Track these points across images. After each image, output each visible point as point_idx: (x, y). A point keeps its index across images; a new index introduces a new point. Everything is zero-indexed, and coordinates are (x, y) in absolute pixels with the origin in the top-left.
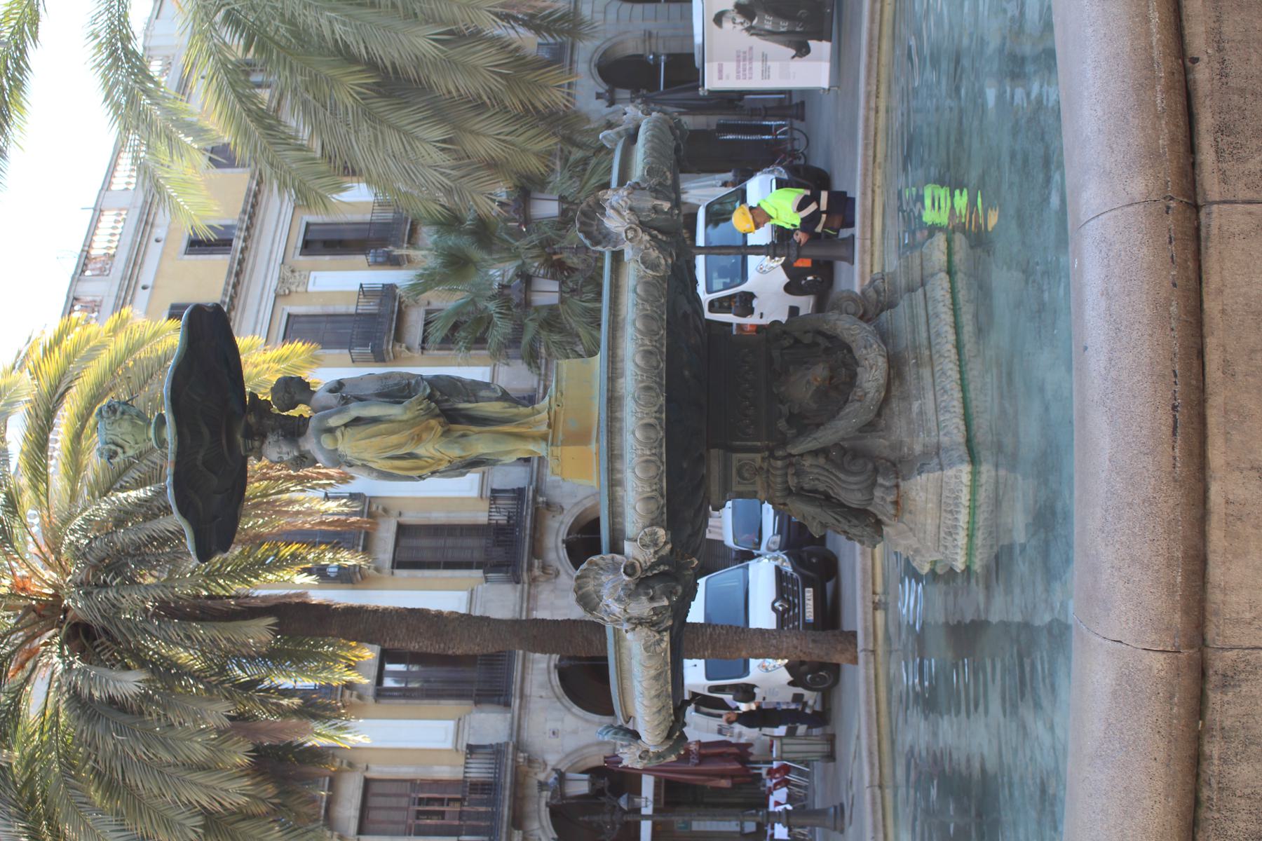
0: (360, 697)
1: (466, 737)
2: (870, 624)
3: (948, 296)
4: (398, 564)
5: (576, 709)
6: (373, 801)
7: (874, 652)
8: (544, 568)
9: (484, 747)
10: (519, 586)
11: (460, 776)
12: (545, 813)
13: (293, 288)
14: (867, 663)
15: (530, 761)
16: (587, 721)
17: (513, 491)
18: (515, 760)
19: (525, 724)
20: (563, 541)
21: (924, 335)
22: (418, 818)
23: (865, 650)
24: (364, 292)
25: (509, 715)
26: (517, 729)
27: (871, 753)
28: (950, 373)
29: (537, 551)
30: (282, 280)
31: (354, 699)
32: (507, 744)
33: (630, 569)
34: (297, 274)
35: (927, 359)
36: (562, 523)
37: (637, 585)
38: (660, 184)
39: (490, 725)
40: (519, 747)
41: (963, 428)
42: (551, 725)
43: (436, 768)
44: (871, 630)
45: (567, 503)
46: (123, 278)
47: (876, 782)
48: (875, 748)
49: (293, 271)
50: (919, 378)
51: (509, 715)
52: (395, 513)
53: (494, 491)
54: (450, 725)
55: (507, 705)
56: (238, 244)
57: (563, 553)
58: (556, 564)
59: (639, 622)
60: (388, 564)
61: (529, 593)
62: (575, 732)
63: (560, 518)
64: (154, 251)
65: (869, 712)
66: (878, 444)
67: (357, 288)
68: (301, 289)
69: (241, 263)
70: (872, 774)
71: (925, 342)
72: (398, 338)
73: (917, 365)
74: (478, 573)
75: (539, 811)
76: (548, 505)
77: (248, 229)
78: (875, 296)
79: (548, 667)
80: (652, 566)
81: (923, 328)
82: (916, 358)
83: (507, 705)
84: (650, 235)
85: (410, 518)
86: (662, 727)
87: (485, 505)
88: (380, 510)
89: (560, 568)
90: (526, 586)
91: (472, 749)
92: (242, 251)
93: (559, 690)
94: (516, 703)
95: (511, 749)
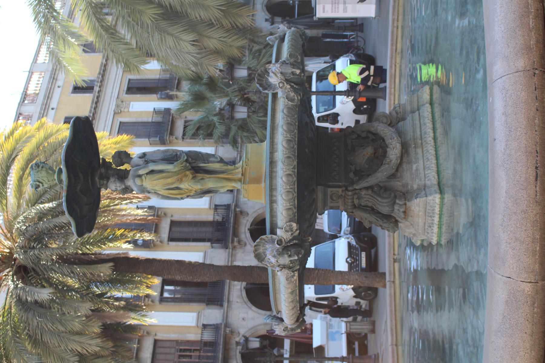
0: (153, 301)
1: (202, 321)
2: (392, 269)
3: (430, 115)
4: (171, 239)
5: (254, 308)
6: (159, 350)
7: (394, 282)
8: (239, 242)
9: (210, 325)
10: (227, 250)
11: (199, 339)
12: (239, 357)
13: (122, 110)
14: (390, 287)
15: (232, 332)
16: (259, 313)
17: (225, 205)
18: (225, 331)
19: (230, 315)
20: (248, 229)
21: (419, 133)
22: (179, 358)
23: (389, 281)
24: (156, 112)
25: (222, 311)
26: (226, 317)
27: (392, 329)
28: (430, 151)
29: (236, 234)
30: (117, 106)
31: (150, 302)
32: (221, 324)
33: (280, 242)
34: (124, 103)
35: (420, 144)
36: (248, 221)
37: (283, 249)
38: (295, 61)
39: (213, 315)
40: (227, 325)
41: (436, 177)
42: (242, 315)
43: (188, 335)
44: (392, 272)
45: (250, 211)
46: (43, 104)
47: (394, 343)
48: (394, 327)
49: (122, 102)
50: (416, 153)
51: (222, 311)
52: (169, 215)
53: (216, 206)
54: (195, 315)
55: (222, 306)
56: (97, 89)
57: (248, 235)
58: (245, 240)
59: (284, 267)
60: (166, 239)
61: (232, 253)
62: (253, 319)
63: (247, 218)
64: (57, 92)
65: (391, 310)
66: (397, 184)
67: (152, 110)
68: (126, 110)
69: (98, 97)
70: (392, 340)
71: (419, 137)
72: (172, 133)
73: (415, 147)
74: (208, 244)
75: (236, 355)
76: (241, 212)
77: (101, 82)
78: (396, 115)
79: (241, 288)
80: (290, 241)
81: (418, 130)
82: (415, 144)
83: (222, 306)
84: (290, 85)
85: (159, 337)
86: (294, 316)
87: (212, 212)
88: (163, 214)
89: (247, 242)
90: (231, 250)
91: (205, 326)
92: (99, 92)
93: (246, 299)
94: (225, 304)
95: (223, 326)
